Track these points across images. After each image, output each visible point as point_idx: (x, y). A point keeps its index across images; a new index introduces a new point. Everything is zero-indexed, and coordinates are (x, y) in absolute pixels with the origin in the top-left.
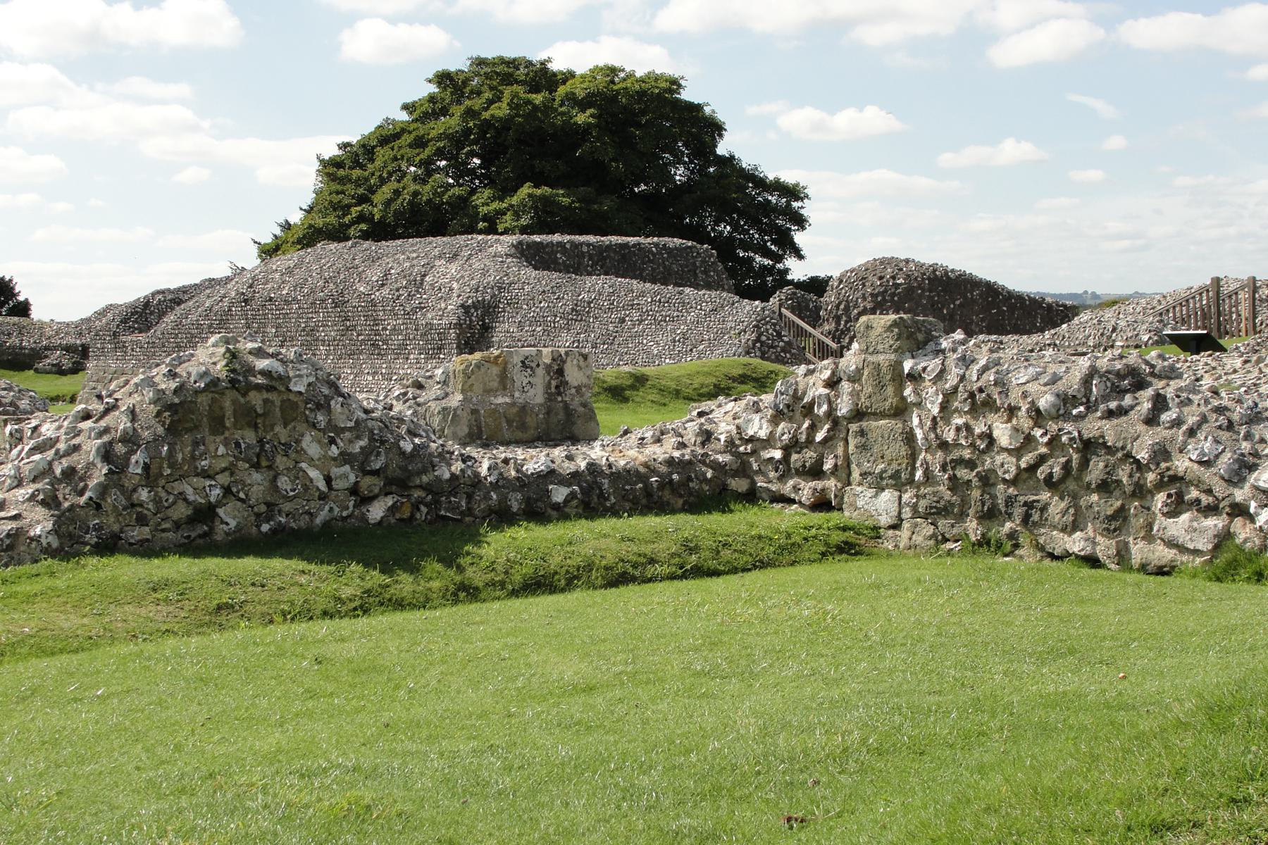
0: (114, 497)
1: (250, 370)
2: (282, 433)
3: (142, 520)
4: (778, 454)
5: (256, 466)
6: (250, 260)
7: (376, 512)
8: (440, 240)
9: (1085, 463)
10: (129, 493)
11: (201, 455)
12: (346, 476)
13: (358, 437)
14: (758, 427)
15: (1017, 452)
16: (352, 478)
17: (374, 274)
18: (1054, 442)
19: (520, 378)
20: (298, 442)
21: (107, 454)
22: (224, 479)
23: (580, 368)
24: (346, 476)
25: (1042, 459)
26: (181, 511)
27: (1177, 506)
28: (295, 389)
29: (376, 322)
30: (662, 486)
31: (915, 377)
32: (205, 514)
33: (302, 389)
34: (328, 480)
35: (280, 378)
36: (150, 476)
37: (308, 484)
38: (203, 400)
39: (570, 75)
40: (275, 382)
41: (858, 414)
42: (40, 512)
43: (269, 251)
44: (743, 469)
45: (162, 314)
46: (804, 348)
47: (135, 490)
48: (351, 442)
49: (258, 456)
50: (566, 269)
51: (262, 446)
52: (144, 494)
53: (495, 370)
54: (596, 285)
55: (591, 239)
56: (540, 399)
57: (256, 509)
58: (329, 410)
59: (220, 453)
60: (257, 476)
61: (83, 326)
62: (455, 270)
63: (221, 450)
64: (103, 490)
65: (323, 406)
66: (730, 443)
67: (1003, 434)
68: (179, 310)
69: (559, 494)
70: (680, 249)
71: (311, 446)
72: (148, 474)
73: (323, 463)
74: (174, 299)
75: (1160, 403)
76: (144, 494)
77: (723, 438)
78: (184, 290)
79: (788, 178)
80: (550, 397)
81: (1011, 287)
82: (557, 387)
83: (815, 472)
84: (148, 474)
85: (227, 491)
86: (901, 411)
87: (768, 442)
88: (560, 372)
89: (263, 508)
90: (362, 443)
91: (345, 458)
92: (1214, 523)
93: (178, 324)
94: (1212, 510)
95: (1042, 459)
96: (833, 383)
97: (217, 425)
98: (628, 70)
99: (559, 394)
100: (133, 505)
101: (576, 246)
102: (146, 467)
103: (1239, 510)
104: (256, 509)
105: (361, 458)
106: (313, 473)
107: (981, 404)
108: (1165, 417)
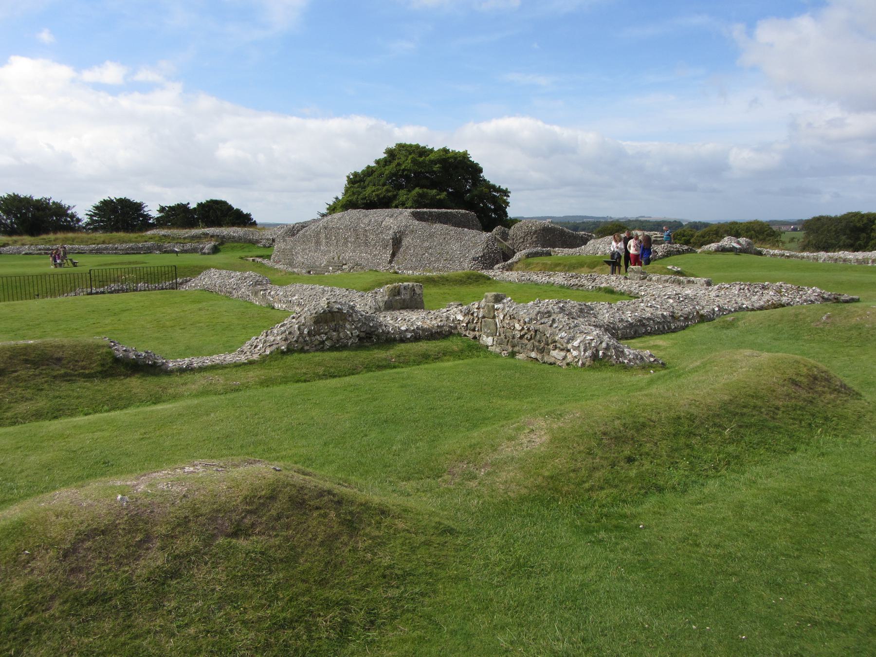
2: (341, 323)
3: (307, 345)
5: (334, 331)
8: (387, 210)
9: (536, 335)
14: (460, 317)
15: (521, 331)
17: (366, 221)
18: (528, 329)
19: (403, 292)
21: (299, 329)
25: (526, 334)
26: (317, 342)
27: (555, 348)
29: (367, 236)
31: (497, 310)
32: (323, 342)
39: (432, 151)
41: (484, 317)
42: (283, 343)
43: (332, 209)
44: (456, 328)
45: (298, 231)
46: (322, 544)
52: (307, 338)
54: (438, 226)
55: (436, 210)
62: (394, 219)
64: (298, 338)
65: (351, 316)
66: (453, 321)
67: (518, 327)
68: (304, 230)
69: (409, 335)
70: (462, 215)
71: (348, 326)
73: (351, 330)
75: (554, 321)
76: (307, 338)
78: (305, 223)
79: (503, 187)
80: (412, 297)
83: (474, 330)
86: (494, 317)
87: (462, 321)
91: (356, 328)
92: (563, 354)
93: (304, 235)
94: (562, 350)
95: (526, 334)
96: (478, 308)
101: (430, 212)
103: (569, 351)
107: (512, 317)
108: (555, 325)
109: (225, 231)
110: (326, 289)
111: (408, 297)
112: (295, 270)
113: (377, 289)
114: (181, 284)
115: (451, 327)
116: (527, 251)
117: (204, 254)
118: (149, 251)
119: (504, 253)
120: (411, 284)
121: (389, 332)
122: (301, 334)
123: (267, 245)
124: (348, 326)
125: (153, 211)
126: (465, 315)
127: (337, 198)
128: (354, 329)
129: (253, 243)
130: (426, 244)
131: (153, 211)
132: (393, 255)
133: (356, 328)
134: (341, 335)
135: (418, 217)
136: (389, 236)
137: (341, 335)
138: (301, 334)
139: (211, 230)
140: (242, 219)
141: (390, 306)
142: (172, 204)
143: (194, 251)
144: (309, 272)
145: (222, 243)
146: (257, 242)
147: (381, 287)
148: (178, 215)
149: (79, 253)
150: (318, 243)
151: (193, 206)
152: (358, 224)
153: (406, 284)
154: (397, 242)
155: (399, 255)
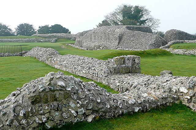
0: (16, 123)
1: (55, 84)
2: (65, 102)
4: (189, 98)
6: (96, 27)
7: (90, 119)
10: (19, 121)
11: (40, 110)
12: (82, 111)
13: (86, 100)
16: (84, 112)
17: (109, 30)
19: (127, 62)
20: (68, 104)
22: (47, 115)
23: (138, 60)
24: (82, 111)
28: (68, 90)
30: (161, 105)
33: (70, 90)
34: (77, 112)
35: (64, 87)
36: (26, 116)
37: (71, 115)
38: (42, 94)
40: (63, 88)
47: (21, 120)
48: (84, 101)
49: (58, 108)
50: (132, 30)
51: (58, 105)
53: (123, 60)
56: (131, 65)
57: (56, 122)
58: (78, 93)
59: (46, 109)
60: (57, 114)
61: (76, 35)
63: (47, 108)
64: (12, 121)
65: (76, 93)
69: (137, 110)
71: (73, 105)
72: (25, 116)
74: (86, 32)
76: (24, 122)
77: (174, 91)
80: (133, 65)
81: (189, 33)
82: (134, 63)
84: (25, 116)
85: (48, 118)
88: (134, 60)
89: (59, 122)
90: (87, 101)
91: (82, 106)
97: (46, 102)
98: (134, 6)
99: (134, 64)
100: (21, 125)
102: (24, 114)
104: (56, 122)
105: (86, 105)
106: (73, 112)
109: (59, 34)
110: (81, 58)
111: (130, 65)
112: (82, 48)
113: (109, 60)
114: (24, 53)
115: (174, 98)
116: (172, 42)
117: (52, 42)
118: (33, 41)
119: (163, 43)
120: (132, 56)
121: (117, 107)
122: (16, 117)
123: (74, 39)
124: (73, 105)
125: (36, 28)
126: (189, 88)
127: (100, 24)
128: (80, 108)
129: (69, 39)
130: (132, 39)
131: (36, 28)
132: (119, 43)
133: (82, 106)
134: (64, 115)
135: (129, 28)
136: (117, 36)
137: (64, 115)
138: (16, 117)
139: (55, 34)
140: (66, 31)
141: (117, 71)
142: (43, 25)
143: (49, 41)
144: (87, 49)
145: (58, 39)
146: (71, 38)
147: (112, 58)
148: (44, 30)
149: (10, 42)
150: (91, 38)
151: (50, 26)
152: (106, 31)
153: (128, 56)
154: (120, 38)
155: (121, 43)
